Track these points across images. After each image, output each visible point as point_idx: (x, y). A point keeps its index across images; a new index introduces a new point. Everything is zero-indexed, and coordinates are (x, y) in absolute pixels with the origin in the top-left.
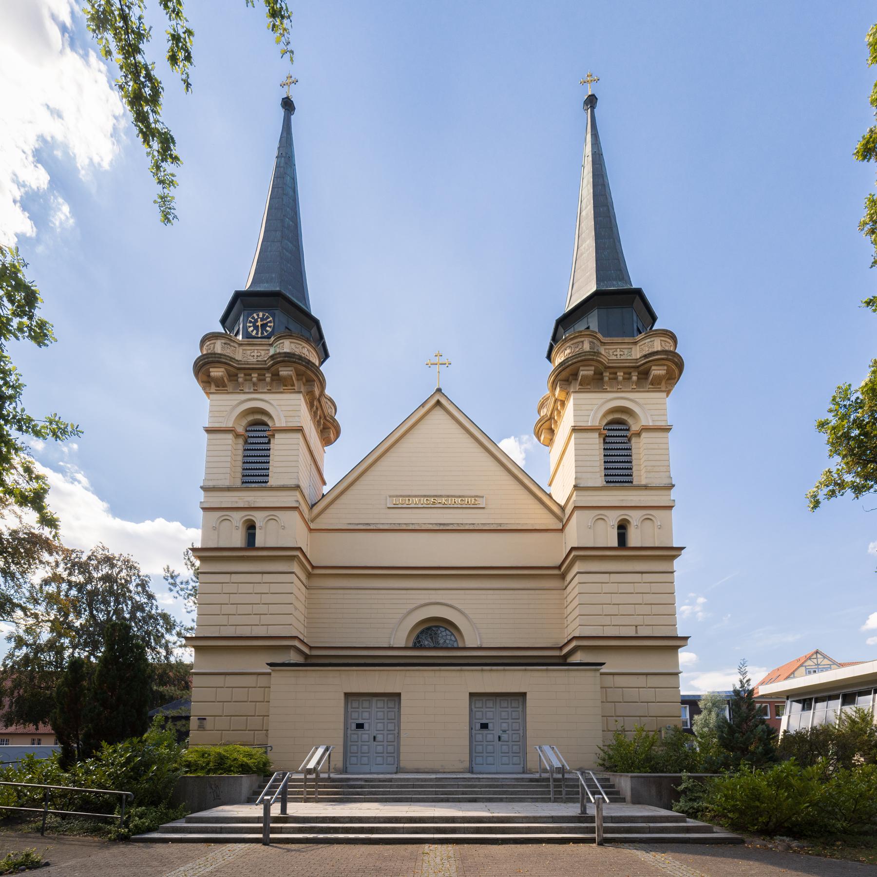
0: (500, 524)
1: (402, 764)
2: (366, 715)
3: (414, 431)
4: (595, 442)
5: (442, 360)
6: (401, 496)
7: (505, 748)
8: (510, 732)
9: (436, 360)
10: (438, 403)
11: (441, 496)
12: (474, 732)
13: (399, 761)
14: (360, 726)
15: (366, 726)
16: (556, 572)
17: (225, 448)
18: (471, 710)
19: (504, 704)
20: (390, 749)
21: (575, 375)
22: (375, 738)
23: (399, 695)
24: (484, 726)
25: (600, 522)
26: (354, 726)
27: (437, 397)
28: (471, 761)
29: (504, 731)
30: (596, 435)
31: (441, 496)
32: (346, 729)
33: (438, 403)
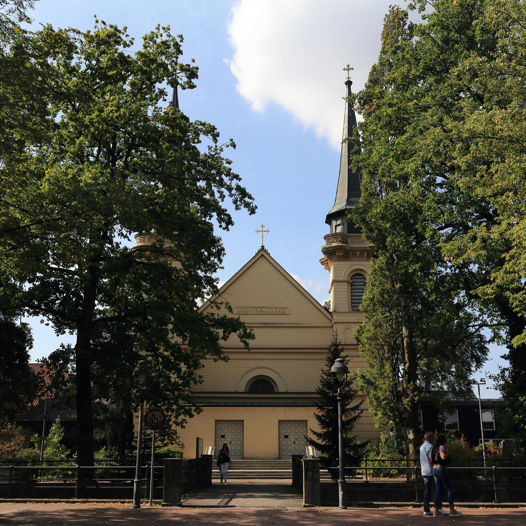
0: (298, 324)
1: (244, 456)
2: (226, 431)
3: (249, 270)
4: (345, 288)
5: (265, 229)
6: (242, 308)
7: (297, 448)
8: (299, 439)
9: (261, 229)
10: (262, 255)
11: (264, 308)
12: (281, 439)
13: (243, 454)
14: (286, 437)
15: (226, 436)
16: (327, 351)
17: (290, 475)
18: (279, 429)
19: (233, 425)
20: (239, 448)
21: (335, 253)
22: (294, 442)
23: (243, 421)
24: (286, 437)
25: (348, 330)
26: (283, 437)
27: (263, 252)
28: (279, 454)
29: (296, 439)
30: (346, 284)
31: (264, 308)
32: (279, 438)
33: (262, 255)
